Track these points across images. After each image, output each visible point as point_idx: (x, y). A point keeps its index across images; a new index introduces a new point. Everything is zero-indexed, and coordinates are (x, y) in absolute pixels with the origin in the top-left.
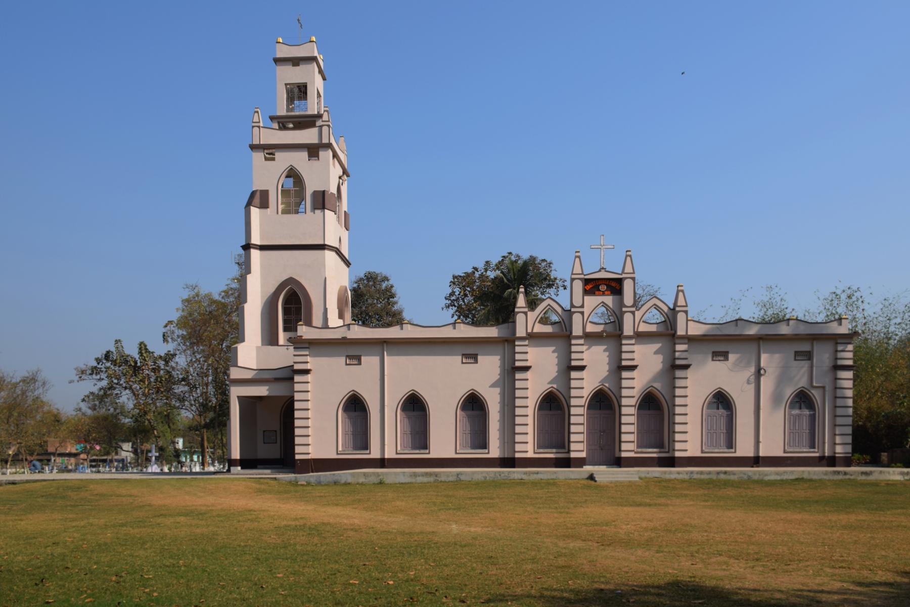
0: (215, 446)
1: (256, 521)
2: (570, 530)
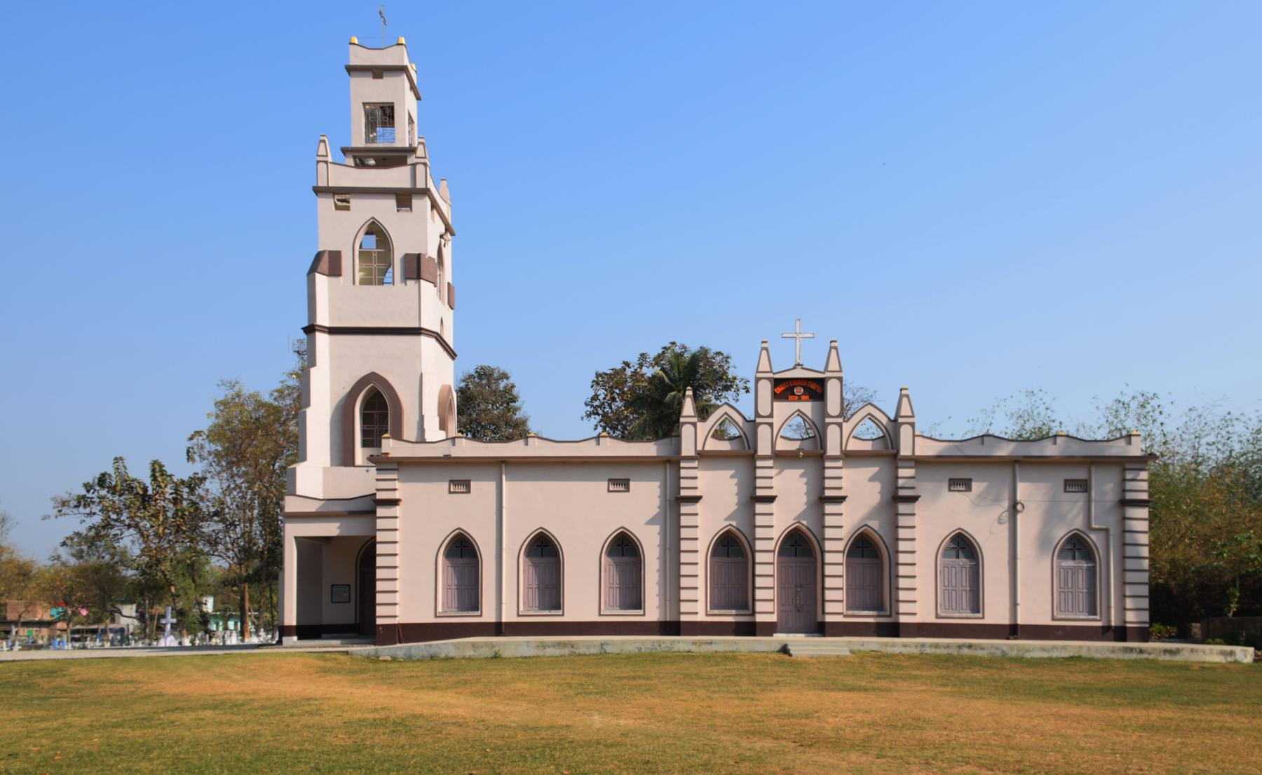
0: (260, 607)
1: (317, 715)
2: (756, 724)
